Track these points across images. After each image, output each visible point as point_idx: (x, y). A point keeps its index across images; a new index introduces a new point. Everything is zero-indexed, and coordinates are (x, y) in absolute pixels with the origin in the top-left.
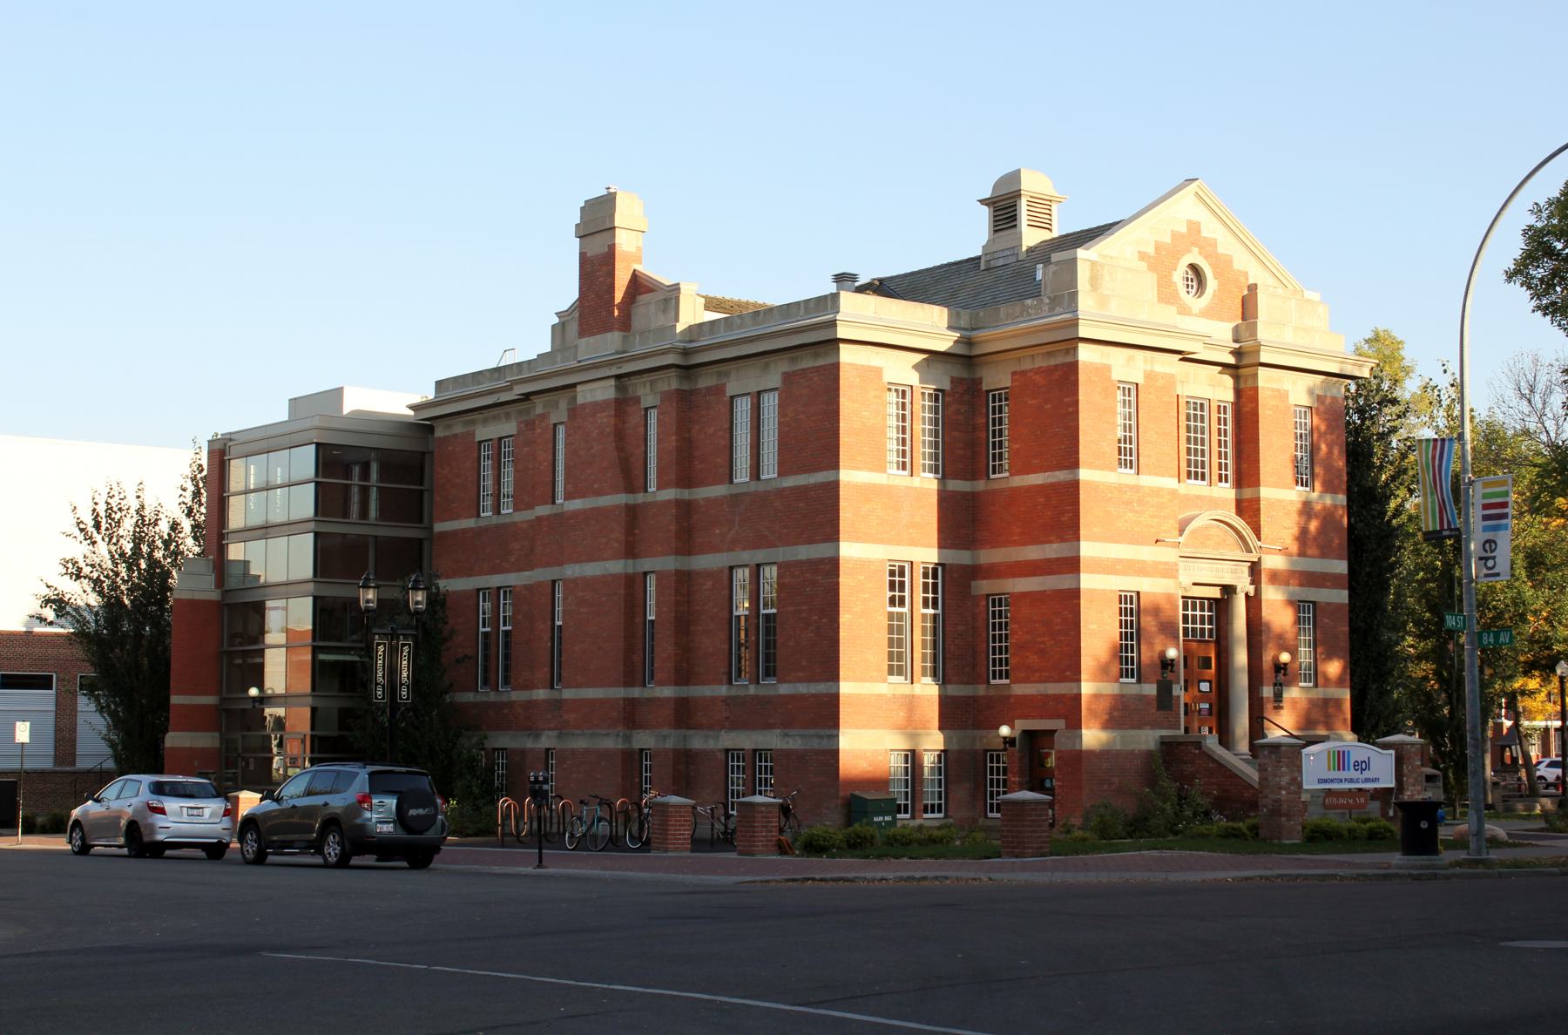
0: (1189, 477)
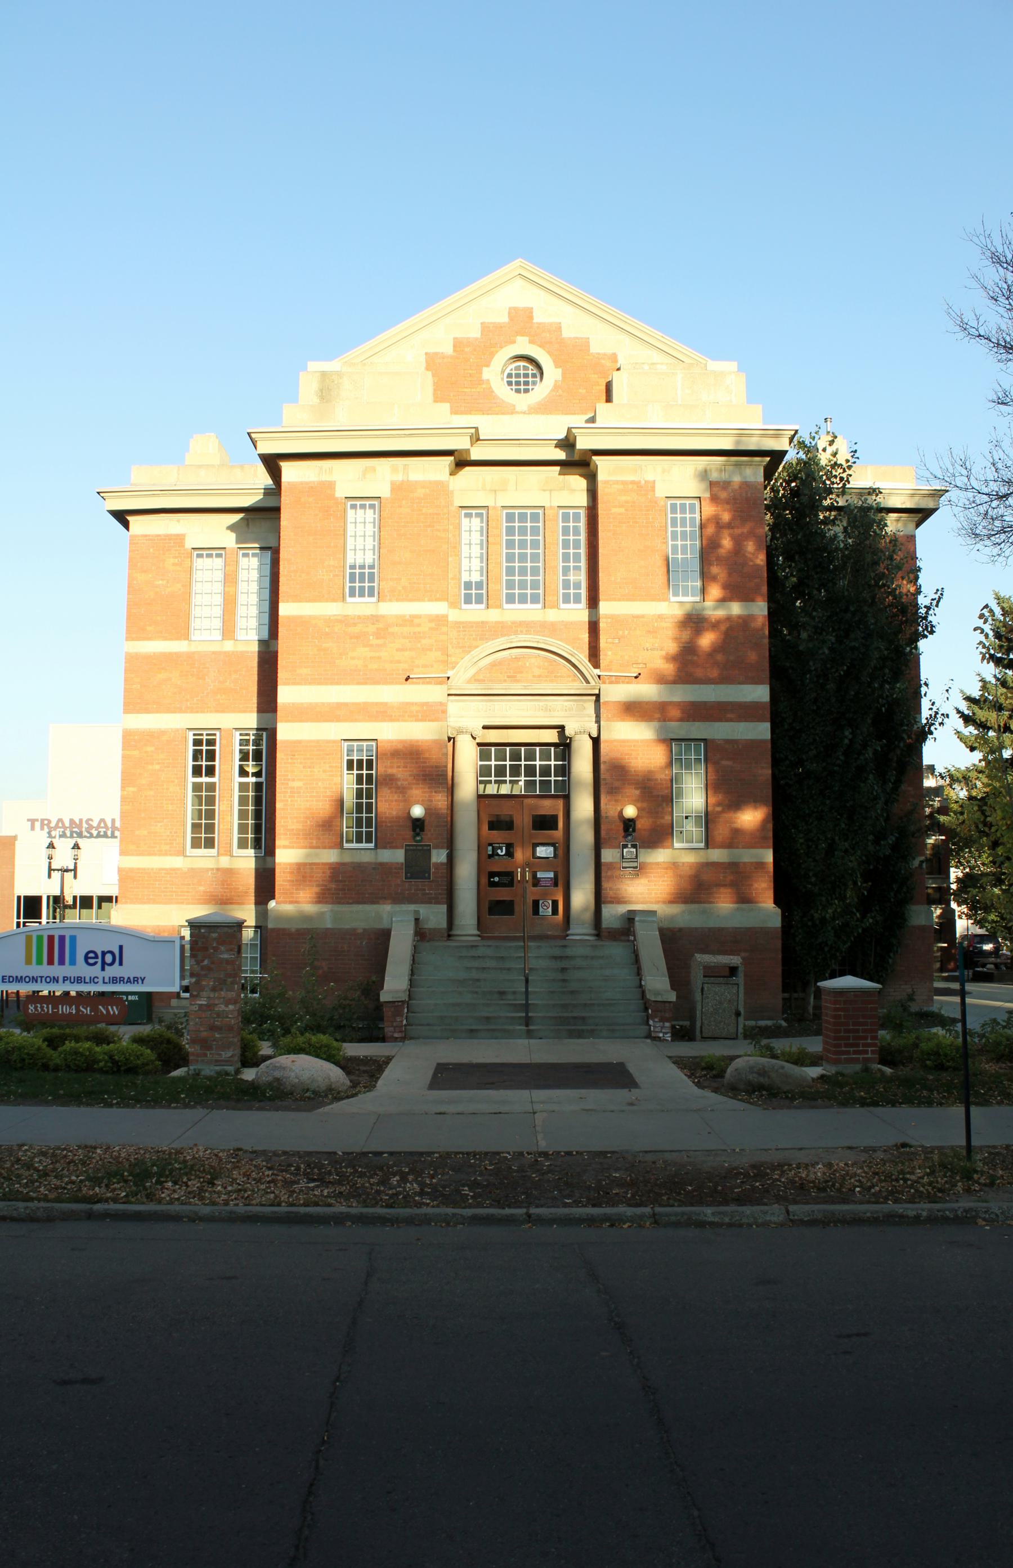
0: (352, 594)
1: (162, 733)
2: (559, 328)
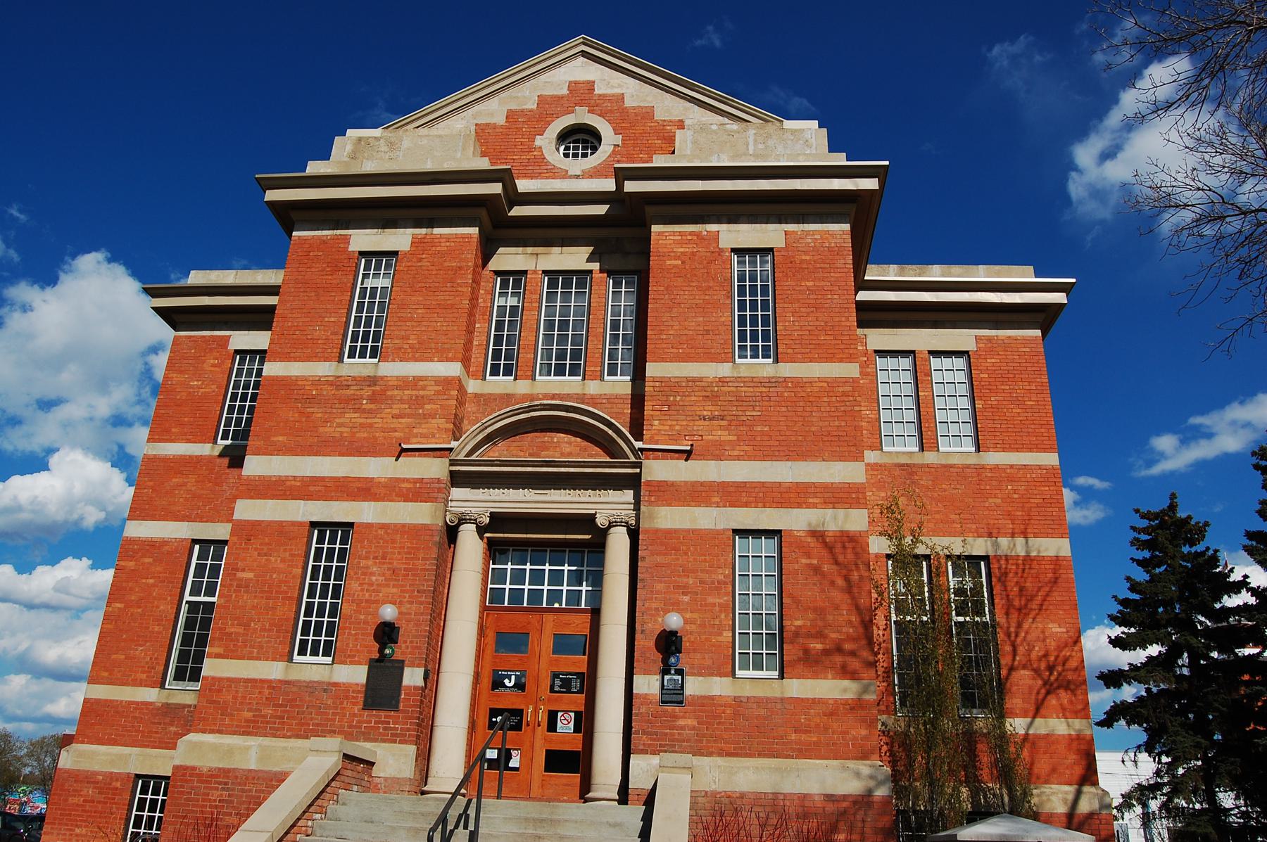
1: (165, 542)
2: (621, 98)
